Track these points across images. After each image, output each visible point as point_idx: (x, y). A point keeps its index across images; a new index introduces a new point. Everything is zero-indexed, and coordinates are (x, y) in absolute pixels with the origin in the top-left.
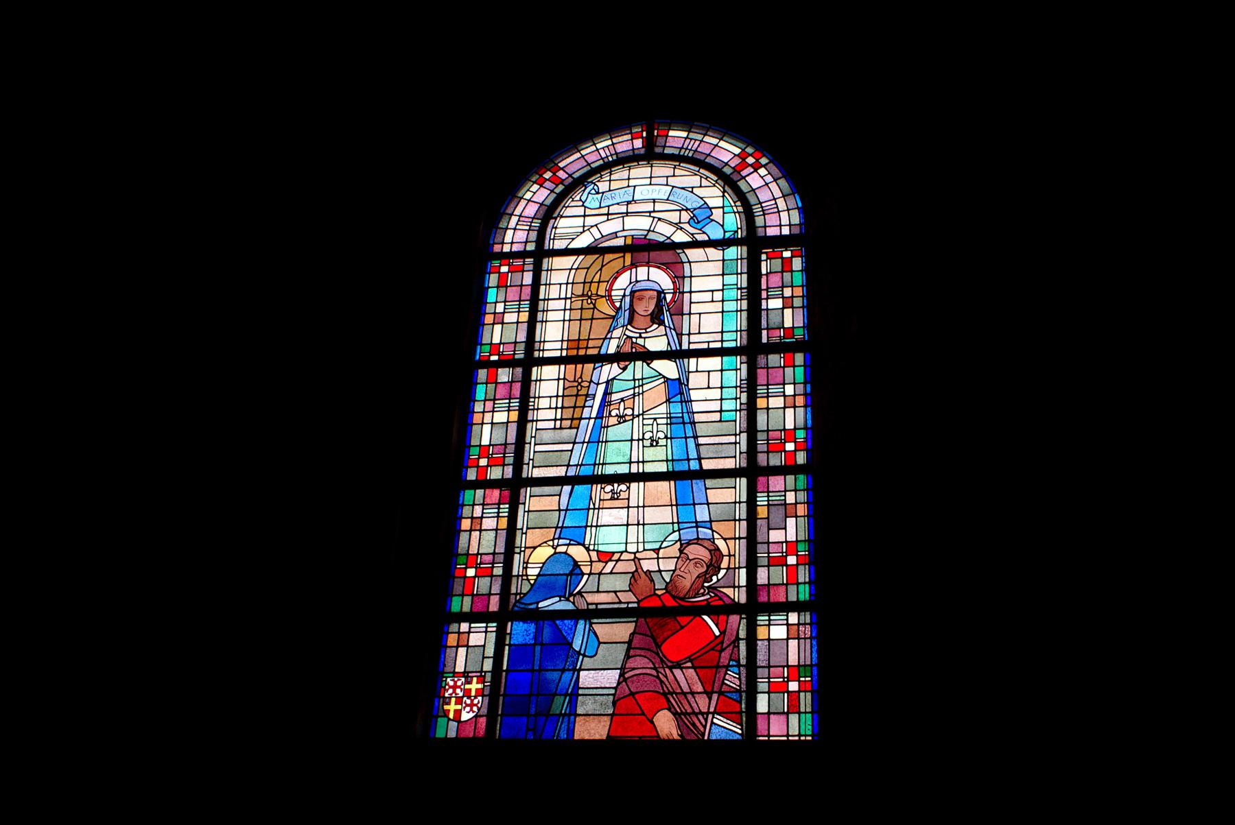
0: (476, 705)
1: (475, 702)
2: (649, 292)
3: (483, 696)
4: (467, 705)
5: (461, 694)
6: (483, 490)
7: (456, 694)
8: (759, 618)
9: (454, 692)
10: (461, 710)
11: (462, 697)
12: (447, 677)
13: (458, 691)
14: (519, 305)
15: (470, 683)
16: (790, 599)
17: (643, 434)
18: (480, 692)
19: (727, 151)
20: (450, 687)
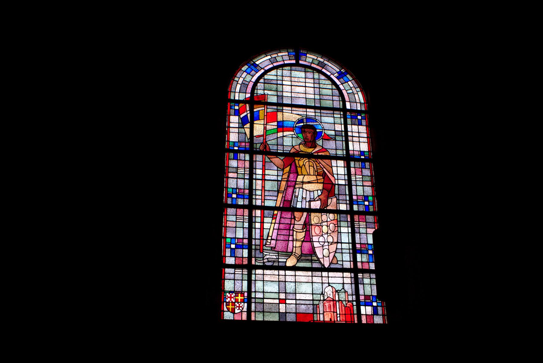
0: (241, 307)
2: (292, 305)
4: (237, 307)
5: (234, 301)
6: (351, 168)
8: (359, 275)
11: (235, 303)
12: (226, 293)
13: (232, 299)
15: (238, 296)
16: (236, 99)
17: (332, 220)
18: (243, 301)
20: (231, 295)
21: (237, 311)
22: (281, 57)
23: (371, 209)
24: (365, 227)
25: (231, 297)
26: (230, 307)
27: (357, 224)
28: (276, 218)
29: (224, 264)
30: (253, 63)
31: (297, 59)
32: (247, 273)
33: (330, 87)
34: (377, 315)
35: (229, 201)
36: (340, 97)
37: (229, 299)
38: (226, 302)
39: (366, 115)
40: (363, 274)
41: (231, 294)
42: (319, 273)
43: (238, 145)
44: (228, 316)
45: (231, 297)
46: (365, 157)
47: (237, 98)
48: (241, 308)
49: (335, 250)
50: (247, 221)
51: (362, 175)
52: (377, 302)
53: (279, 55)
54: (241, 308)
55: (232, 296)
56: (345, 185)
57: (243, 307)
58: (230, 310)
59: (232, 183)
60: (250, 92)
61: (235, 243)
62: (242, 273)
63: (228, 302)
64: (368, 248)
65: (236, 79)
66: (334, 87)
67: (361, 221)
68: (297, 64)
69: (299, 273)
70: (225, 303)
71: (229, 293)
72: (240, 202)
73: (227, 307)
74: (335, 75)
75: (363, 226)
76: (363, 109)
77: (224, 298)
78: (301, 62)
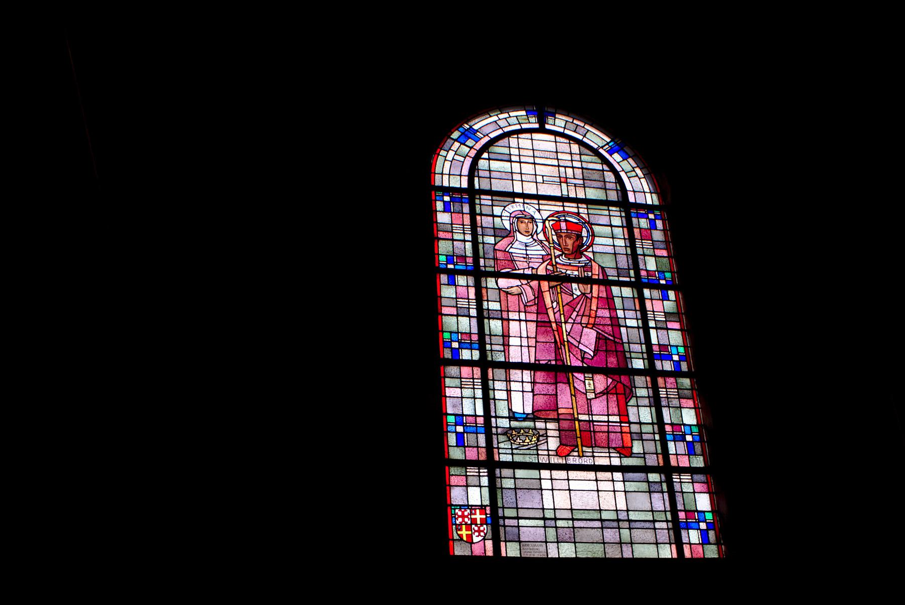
0: (483, 531)
1: (482, 528)
3: (487, 524)
4: (476, 531)
7: (468, 514)
9: (467, 517)
10: (472, 534)
12: (455, 509)
13: (466, 520)
14: (469, 305)
15: (475, 514)
16: (444, 185)
18: (483, 522)
19: (597, 138)
20: (463, 513)
21: (476, 539)
22: (515, 118)
23: (684, 367)
24: (691, 481)
25: (463, 516)
26: (464, 533)
27: (651, 314)
28: (514, 269)
29: (436, 267)
30: (468, 127)
31: (542, 122)
32: (475, 307)
33: (599, 167)
34: (656, 229)
35: (448, 354)
36: (617, 184)
37: (460, 520)
38: (456, 524)
39: (662, 212)
40: (680, 476)
41: (463, 510)
42: (608, 475)
43: (458, 338)
44: (459, 550)
45: (463, 516)
46: (666, 281)
47: (446, 184)
48: (482, 534)
49: (622, 385)
50: (486, 474)
51: (677, 388)
52: (692, 435)
53: (511, 115)
54: (482, 534)
55: (466, 513)
56: (638, 328)
57: (485, 531)
58: (465, 538)
59: (449, 323)
60: (467, 173)
61: (459, 340)
62: (479, 474)
63: (459, 525)
64: (684, 432)
65: (443, 153)
66: (606, 168)
67: (662, 350)
68: (542, 130)
69: (573, 474)
70: (454, 526)
71: (460, 509)
72: (466, 355)
73: (459, 532)
74: (604, 148)
75: (674, 395)
76: (656, 203)
77: (452, 517)
78: (547, 127)
